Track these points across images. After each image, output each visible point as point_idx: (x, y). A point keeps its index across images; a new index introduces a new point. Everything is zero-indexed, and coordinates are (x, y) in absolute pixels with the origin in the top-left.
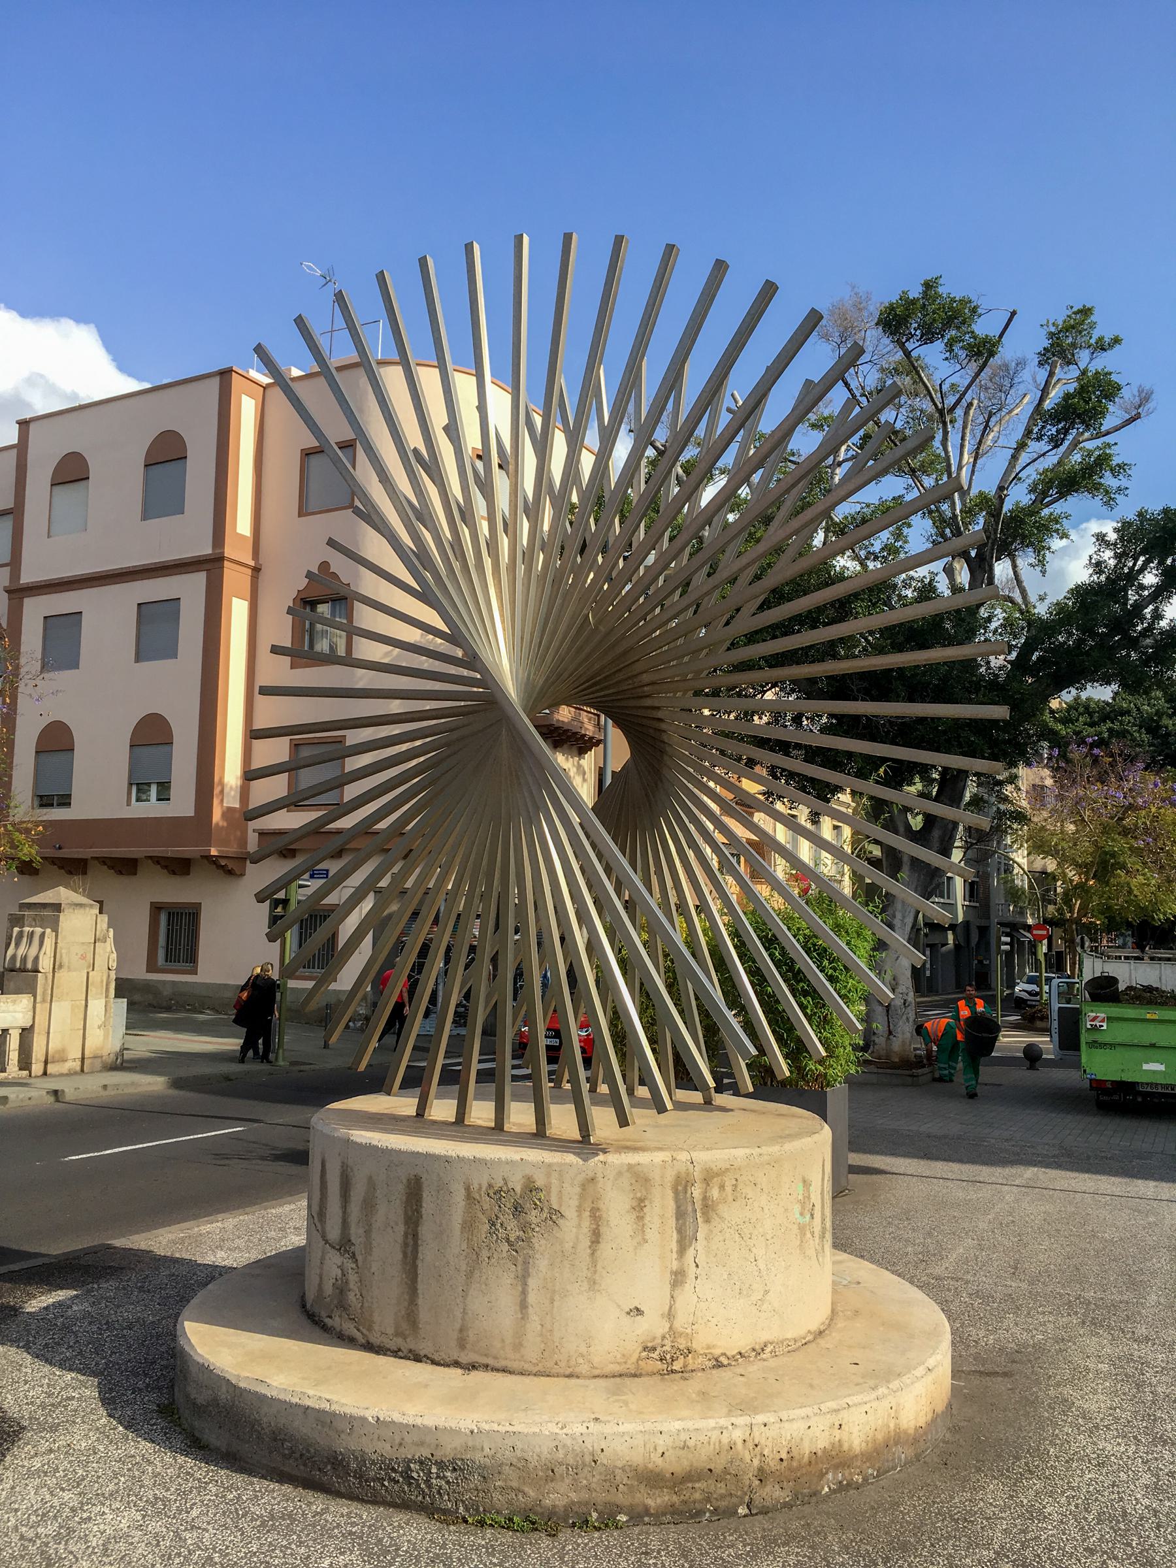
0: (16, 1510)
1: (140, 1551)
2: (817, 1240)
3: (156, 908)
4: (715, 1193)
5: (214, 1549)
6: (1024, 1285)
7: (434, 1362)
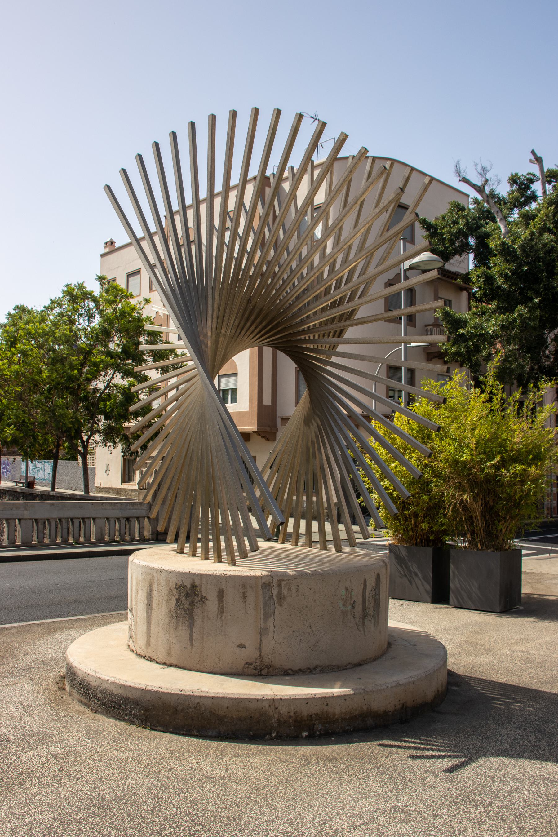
4: (285, 591)
7: (157, 663)
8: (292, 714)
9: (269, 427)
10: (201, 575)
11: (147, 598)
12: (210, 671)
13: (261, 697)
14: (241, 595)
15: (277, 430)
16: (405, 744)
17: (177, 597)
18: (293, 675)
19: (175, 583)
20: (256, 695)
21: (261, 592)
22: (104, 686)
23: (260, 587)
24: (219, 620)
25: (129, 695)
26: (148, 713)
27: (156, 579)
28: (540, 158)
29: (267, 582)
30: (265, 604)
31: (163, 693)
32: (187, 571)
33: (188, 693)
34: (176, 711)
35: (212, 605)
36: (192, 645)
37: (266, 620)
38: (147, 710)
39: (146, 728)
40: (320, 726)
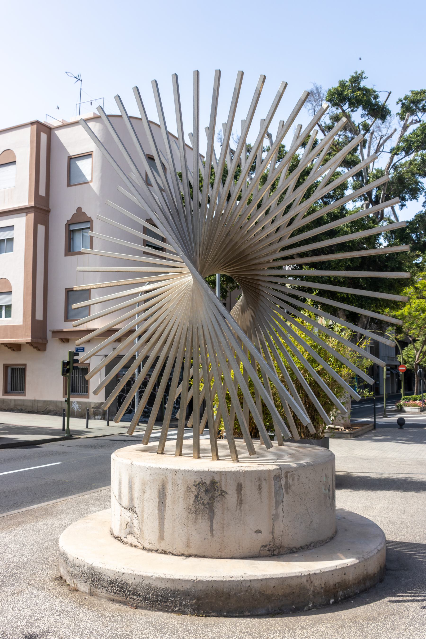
0: (6, 617)
1: (62, 630)
2: (331, 500)
3: (6, 367)
4: (290, 481)
5: (93, 629)
6: (409, 518)
7: (173, 554)
8: (323, 586)
9: (41, 338)
10: (221, 472)
11: (159, 497)
12: (230, 557)
13: (300, 574)
14: (257, 487)
15: (47, 341)
16: (401, 599)
17: (196, 493)
18: (297, 552)
19: (193, 481)
20: (295, 573)
21: (273, 483)
22: (146, 582)
23: (272, 479)
24: (238, 511)
25: (179, 587)
26: (200, 602)
27: (170, 479)
28: (271, 134)
29: (278, 475)
30: (276, 493)
31: (215, 581)
32: (206, 469)
33: (239, 579)
34: (228, 596)
35: (232, 498)
36: (212, 535)
37: (277, 508)
38: (199, 599)
39: (199, 616)
40: (341, 593)
